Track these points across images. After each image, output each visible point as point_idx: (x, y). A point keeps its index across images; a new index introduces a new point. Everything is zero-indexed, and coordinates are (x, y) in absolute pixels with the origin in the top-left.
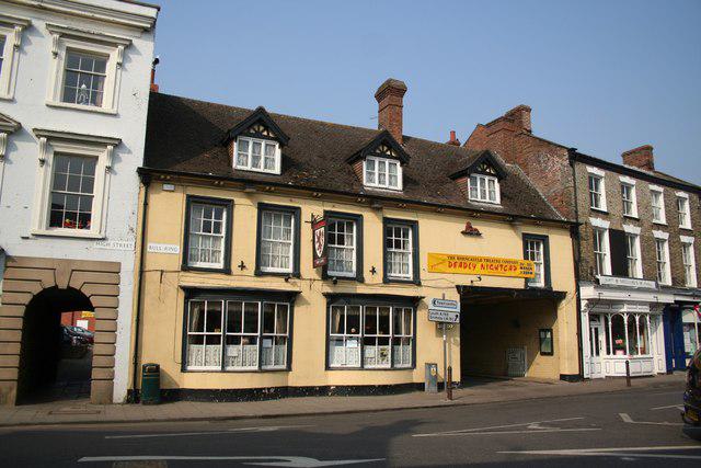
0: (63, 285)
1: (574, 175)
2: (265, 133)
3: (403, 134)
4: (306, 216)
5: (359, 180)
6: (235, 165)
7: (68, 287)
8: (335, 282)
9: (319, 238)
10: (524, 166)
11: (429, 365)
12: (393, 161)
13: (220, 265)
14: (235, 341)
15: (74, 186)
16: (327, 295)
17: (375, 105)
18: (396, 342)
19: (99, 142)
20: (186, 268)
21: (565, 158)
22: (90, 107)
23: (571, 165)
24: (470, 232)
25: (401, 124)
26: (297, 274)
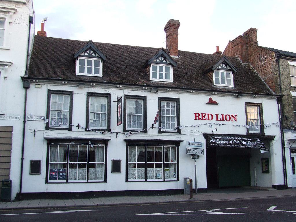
1: (279, 67)
2: (164, 61)
3: (179, 49)
4: (113, 98)
5: (147, 75)
6: (151, 79)
10: (253, 63)
11: (185, 179)
12: (228, 72)
14: (151, 166)
16: (125, 141)
17: (164, 34)
18: (167, 166)
20: (47, 128)
23: (278, 61)
24: (211, 102)
25: (177, 44)
26: (109, 130)
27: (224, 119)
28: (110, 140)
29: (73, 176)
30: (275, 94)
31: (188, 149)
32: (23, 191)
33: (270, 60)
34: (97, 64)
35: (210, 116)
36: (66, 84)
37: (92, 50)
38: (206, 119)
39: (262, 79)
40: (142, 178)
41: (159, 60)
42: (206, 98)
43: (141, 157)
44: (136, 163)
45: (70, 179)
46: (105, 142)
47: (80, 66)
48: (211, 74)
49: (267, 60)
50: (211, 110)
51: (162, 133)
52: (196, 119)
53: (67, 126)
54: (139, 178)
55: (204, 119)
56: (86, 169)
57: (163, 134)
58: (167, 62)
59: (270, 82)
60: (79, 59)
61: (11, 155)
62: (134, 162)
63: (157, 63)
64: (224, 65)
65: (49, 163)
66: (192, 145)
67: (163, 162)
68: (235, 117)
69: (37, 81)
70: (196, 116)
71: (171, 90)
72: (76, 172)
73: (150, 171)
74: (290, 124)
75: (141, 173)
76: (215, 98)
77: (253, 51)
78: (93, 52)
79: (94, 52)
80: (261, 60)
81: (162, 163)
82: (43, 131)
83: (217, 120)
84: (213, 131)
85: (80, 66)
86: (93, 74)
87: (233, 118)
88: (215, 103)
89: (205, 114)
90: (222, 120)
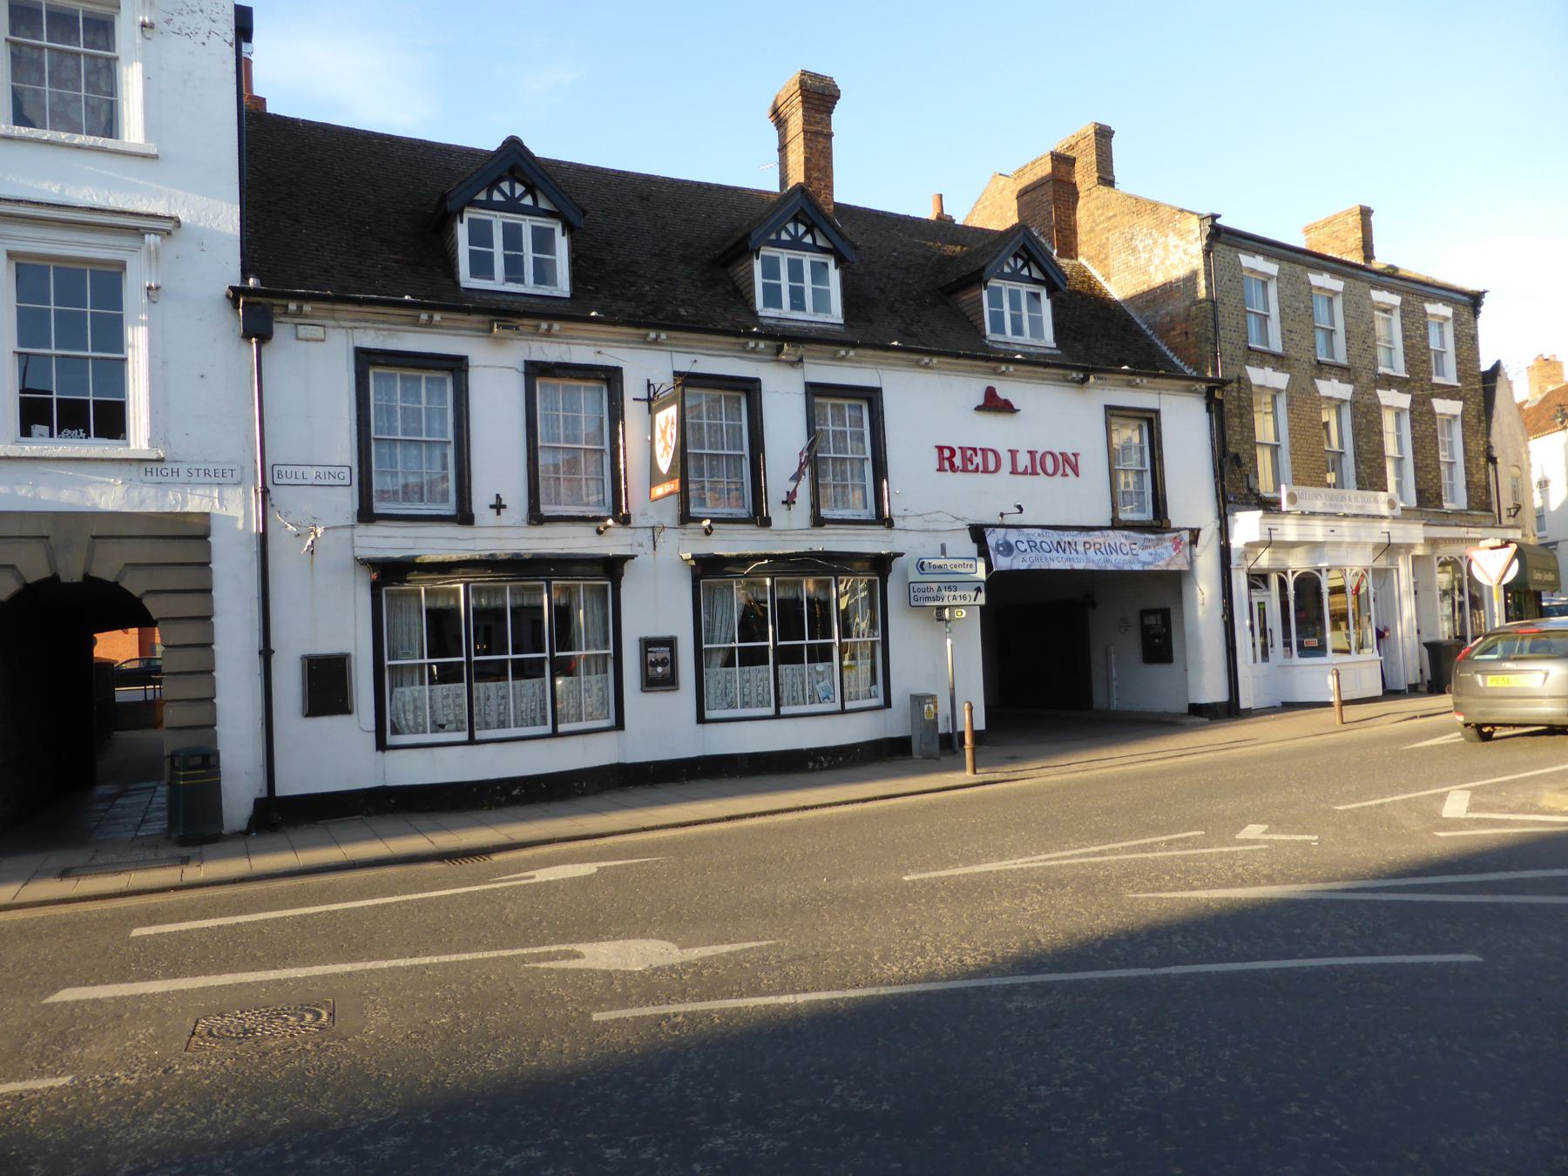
0: (72, 572)
2: (528, 201)
4: (632, 388)
7: (87, 577)
8: (708, 532)
9: (664, 432)
11: (918, 700)
13: (450, 508)
14: (494, 673)
15: (71, 332)
19: (132, 226)
20: (366, 515)
21: (1192, 237)
22: (100, 141)
24: (994, 404)
27: (1039, 470)
28: (632, 557)
29: (494, 714)
30: (1195, 374)
31: (916, 586)
32: (282, 790)
33: (1176, 247)
34: (543, 241)
35: (991, 456)
36: (850, 360)
37: (522, 183)
38: (977, 470)
39: (1139, 321)
40: (761, 703)
41: (502, 193)
42: (968, 387)
43: (751, 624)
44: (733, 648)
45: (483, 725)
46: (613, 567)
47: (507, 252)
48: (745, 265)
49: (1166, 249)
50: (992, 432)
51: (827, 526)
52: (941, 469)
53: (447, 508)
54: (745, 704)
55: (971, 467)
56: (543, 684)
57: (828, 531)
58: (820, 242)
59: (1173, 329)
60: (466, 217)
61: (212, 636)
62: (725, 643)
63: (490, 205)
64: (1020, 263)
65: (387, 663)
66: (932, 570)
67: (547, 654)
68: (1073, 458)
69: (307, 308)
70: (941, 459)
71: (663, 336)
72: (503, 697)
73: (790, 677)
74: (1245, 484)
75: (754, 685)
76: (1005, 390)
77: (1100, 212)
78: (523, 188)
79: (530, 190)
80: (1134, 250)
81: (544, 658)
82: (348, 531)
83: (1014, 472)
84: (1002, 515)
85: (507, 252)
86: (529, 286)
87: (1067, 465)
88: (1006, 408)
89: (974, 450)
90: (981, 468)
